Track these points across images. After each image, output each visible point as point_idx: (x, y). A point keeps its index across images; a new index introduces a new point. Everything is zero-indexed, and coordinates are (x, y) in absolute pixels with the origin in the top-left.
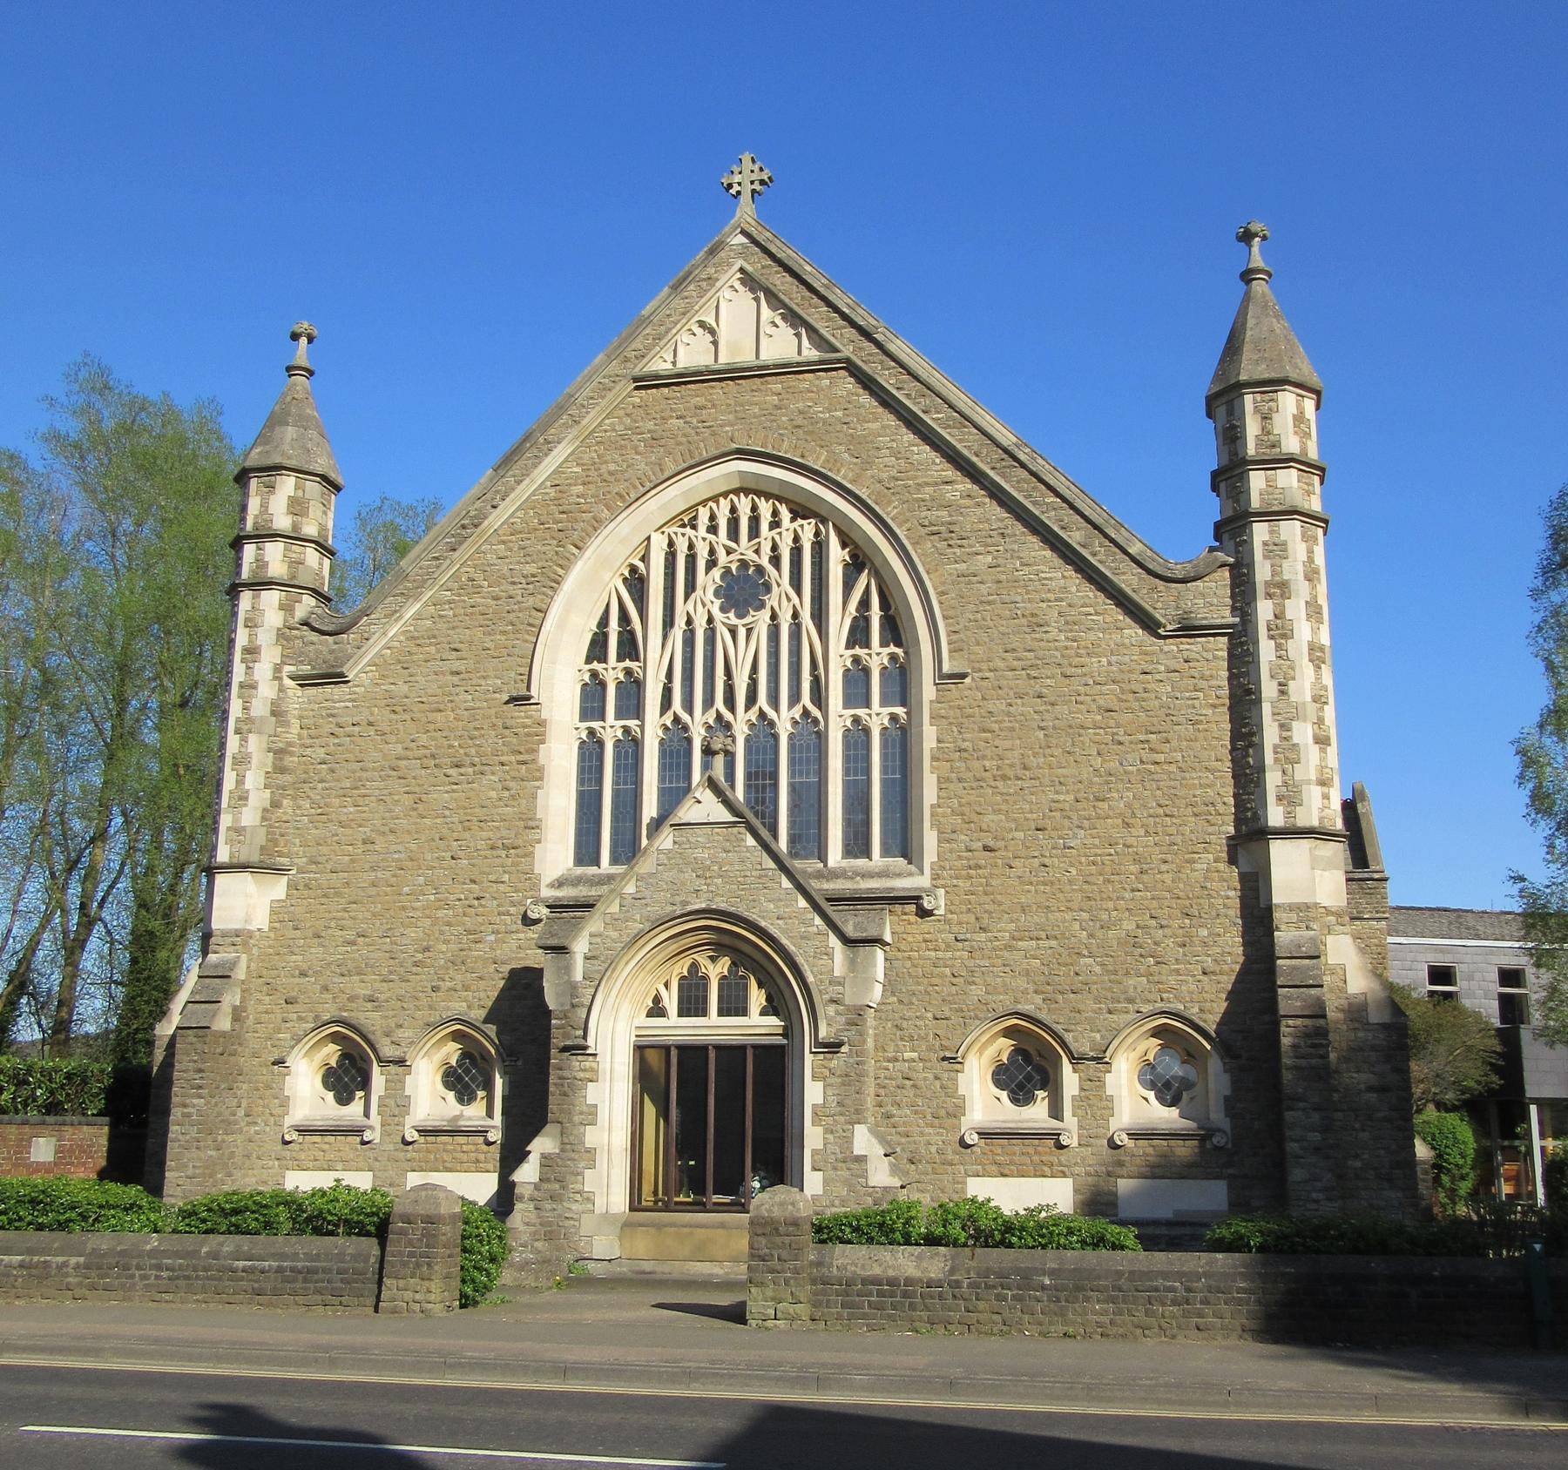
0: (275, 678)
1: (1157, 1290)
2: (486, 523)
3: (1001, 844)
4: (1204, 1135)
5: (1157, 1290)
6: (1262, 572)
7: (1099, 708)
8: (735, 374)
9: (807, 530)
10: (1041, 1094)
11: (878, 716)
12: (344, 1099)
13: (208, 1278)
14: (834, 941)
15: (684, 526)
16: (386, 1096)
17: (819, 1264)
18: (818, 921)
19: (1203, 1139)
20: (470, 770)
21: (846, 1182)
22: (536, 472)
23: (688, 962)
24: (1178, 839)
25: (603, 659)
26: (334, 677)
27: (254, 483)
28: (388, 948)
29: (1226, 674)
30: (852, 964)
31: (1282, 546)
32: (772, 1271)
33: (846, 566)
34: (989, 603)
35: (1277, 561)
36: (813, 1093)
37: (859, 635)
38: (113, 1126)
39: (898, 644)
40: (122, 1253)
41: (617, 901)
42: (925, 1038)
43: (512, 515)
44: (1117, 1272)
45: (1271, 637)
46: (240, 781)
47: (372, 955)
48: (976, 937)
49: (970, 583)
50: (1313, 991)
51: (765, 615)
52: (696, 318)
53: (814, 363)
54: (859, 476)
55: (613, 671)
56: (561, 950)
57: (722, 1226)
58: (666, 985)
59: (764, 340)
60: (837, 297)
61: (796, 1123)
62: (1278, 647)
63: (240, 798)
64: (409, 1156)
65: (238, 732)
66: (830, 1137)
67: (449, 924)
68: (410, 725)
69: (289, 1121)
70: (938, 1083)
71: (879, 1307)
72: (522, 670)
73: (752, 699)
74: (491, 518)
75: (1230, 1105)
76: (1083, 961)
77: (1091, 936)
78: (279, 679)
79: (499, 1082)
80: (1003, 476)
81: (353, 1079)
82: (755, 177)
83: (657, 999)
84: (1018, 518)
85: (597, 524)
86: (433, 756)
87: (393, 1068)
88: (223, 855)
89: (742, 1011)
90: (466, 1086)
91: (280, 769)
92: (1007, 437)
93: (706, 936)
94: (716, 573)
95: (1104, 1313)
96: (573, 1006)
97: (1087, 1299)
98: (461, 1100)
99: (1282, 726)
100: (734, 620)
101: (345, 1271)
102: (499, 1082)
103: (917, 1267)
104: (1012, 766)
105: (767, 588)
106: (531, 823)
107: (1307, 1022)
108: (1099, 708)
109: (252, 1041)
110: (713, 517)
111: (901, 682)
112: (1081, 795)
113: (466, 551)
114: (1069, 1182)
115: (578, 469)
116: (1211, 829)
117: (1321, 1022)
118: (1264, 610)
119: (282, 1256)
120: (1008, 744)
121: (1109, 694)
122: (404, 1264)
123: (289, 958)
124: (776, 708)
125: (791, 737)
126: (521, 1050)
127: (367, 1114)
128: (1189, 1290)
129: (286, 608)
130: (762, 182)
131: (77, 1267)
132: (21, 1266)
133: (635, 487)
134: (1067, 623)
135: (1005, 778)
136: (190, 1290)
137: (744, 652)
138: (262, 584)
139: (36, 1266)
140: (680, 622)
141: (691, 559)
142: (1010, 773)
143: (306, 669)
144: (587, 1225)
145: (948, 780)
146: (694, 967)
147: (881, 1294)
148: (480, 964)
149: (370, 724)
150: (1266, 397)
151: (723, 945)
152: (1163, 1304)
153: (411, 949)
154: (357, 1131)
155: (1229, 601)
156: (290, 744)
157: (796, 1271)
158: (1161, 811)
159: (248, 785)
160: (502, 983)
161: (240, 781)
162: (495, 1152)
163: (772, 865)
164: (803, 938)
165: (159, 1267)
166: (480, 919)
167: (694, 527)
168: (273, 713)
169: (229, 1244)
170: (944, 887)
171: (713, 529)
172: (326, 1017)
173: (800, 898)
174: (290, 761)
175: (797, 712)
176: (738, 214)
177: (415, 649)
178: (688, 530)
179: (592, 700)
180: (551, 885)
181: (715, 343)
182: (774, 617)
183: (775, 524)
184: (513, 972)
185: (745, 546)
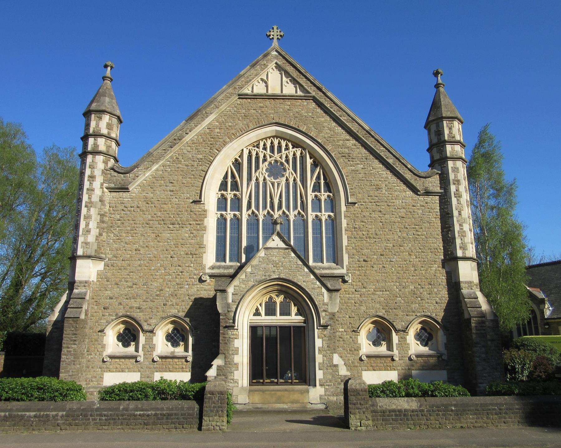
0: (101, 188)
1: (490, 410)
2: (184, 139)
3: (369, 260)
4: (439, 356)
5: (490, 410)
6: (452, 176)
7: (400, 216)
8: (274, 97)
9: (298, 152)
10: (384, 343)
11: (324, 215)
12: (126, 344)
13: (123, 419)
14: (324, 290)
15: (254, 147)
16: (146, 344)
17: (373, 405)
18: (318, 283)
19: (438, 357)
20: (178, 226)
21: (331, 374)
22: (203, 123)
23: (268, 296)
24: (426, 260)
25: (226, 190)
26: (124, 189)
27: (93, 116)
28: (146, 289)
29: (439, 208)
30: (330, 298)
31: (458, 169)
32: (358, 409)
33: (312, 164)
34: (362, 180)
35: (456, 173)
36: (318, 343)
37: (316, 188)
38: (6, 356)
39: (330, 192)
40: (83, 410)
41: (244, 274)
42: (346, 324)
43: (193, 137)
44: (476, 404)
45: (455, 197)
46: (87, 225)
47: (139, 292)
48: (362, 290)
49: (356, 173)
50: (479, 309)
51: (284, 179)
52: (260, 77)
53: (300, 96)
54: (317, 135)
55: (230, 194)
56: (224, 291)
57: (286, 390)
58: (260, 305)
59: (284, 87)
60: (308, 75)
61: (311, 354)
62: (458, 200)
63: (87, 231)
64: (155, 366)
65: (86, 206)
66: (325, 358)
67: (170, 281)
68: (155, 209)
69: (105, 354)
70: (351, 339)
71: (396, 420)
72: (197, 192)
73: (280, 207)
74: (186, 137)
75: (446, 346)
76: (398, 299)
77: (400, 290)
78: (103, 188)
79: (191, 339)
80: (366, 139)
81: (129, 338)
82: (278, 33)
83: (257, 310)
84: (371, 153)
85: (225, 144)
86: (163, 220)
87: (148, 334)
88: (80, 252)
89: (289, 314)
90: (175, 341)
91: (102, 222)
92: (367, 128)
93: (276, 287)
94: (267, 163)
95: (473, 418)
96: (228, 311)
97: (467, 414)
98: (173, 345)
99: (460, 225)
100: (273, 180)
101: (185, 414)
102: (191, 339)
103: (408, 405)
104: (372, 234)
105: (285, 170)
106: (202, 246)
107: (480, 319)
108: (400, 216)
109: (90, 323)
110: (265, 145)
111: (333, 204)
112: (395, 245)
113: (176, 148)
114: (396, 372)
115: (218, 124)
116: (436, 257)
117: (484, 319)
118: (453, 188)
119: (158, 409)
120: (370, 227)
121: (402, 212)
122: (212, 411)
123: (104, 292)
124: (289, 210)
125: (294, 221)
126: (204, 326)
127: (137, 350)
128: (500, 409)
129: (105, 162)
130: (281, 36)
131: (62, 416)
132: (35, 416)
133: (239, 132)
134: (388, 188)
135: (370, 238)
136: (115, 424)
137: (278, 190)
138: (96, 152)
139: (43, 416)
140: (254, 179)
141: (257, 158)
142: (372, 236)
143: (112, 185)
144: (235, 392)
145: (351, 238)
146: (271, 298)
147: (396, 415)
148: (182, 296)
149: (138, 207)
150: (450, 122)
151: (282, 291)
152: (492, 415)
153: (155, 290)
154: (135, 357)
155: (439, 185)
156: (106, 212)
157: (367, 409)
158: (420, 251)
159: (91, 226)
160: (191, 303)
161: (87, 225)
162: (189, 365)
163: (301, 263)
164: (312, 289)
165: (101, 415)
166: (182, 280)
167: (258, 148)
168: (100, 201)
169: (132, 405)
170: (351, 273)
171: (265, 149)
172: (121, 314)
173: (311, 275)
174: (106, 219)
175: (296, 212)
176: (273, 45)
177: (156, 182)
178: (256, 148)
179: (222, 203)
180: (210, 268)
181: (267, 86)
182: (287, 180)
183: (287, 149)
184: (195, 299)
185: (277, 156)
